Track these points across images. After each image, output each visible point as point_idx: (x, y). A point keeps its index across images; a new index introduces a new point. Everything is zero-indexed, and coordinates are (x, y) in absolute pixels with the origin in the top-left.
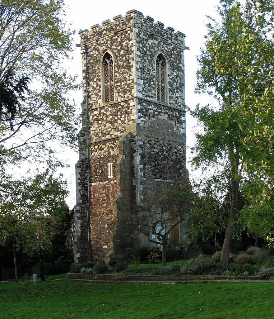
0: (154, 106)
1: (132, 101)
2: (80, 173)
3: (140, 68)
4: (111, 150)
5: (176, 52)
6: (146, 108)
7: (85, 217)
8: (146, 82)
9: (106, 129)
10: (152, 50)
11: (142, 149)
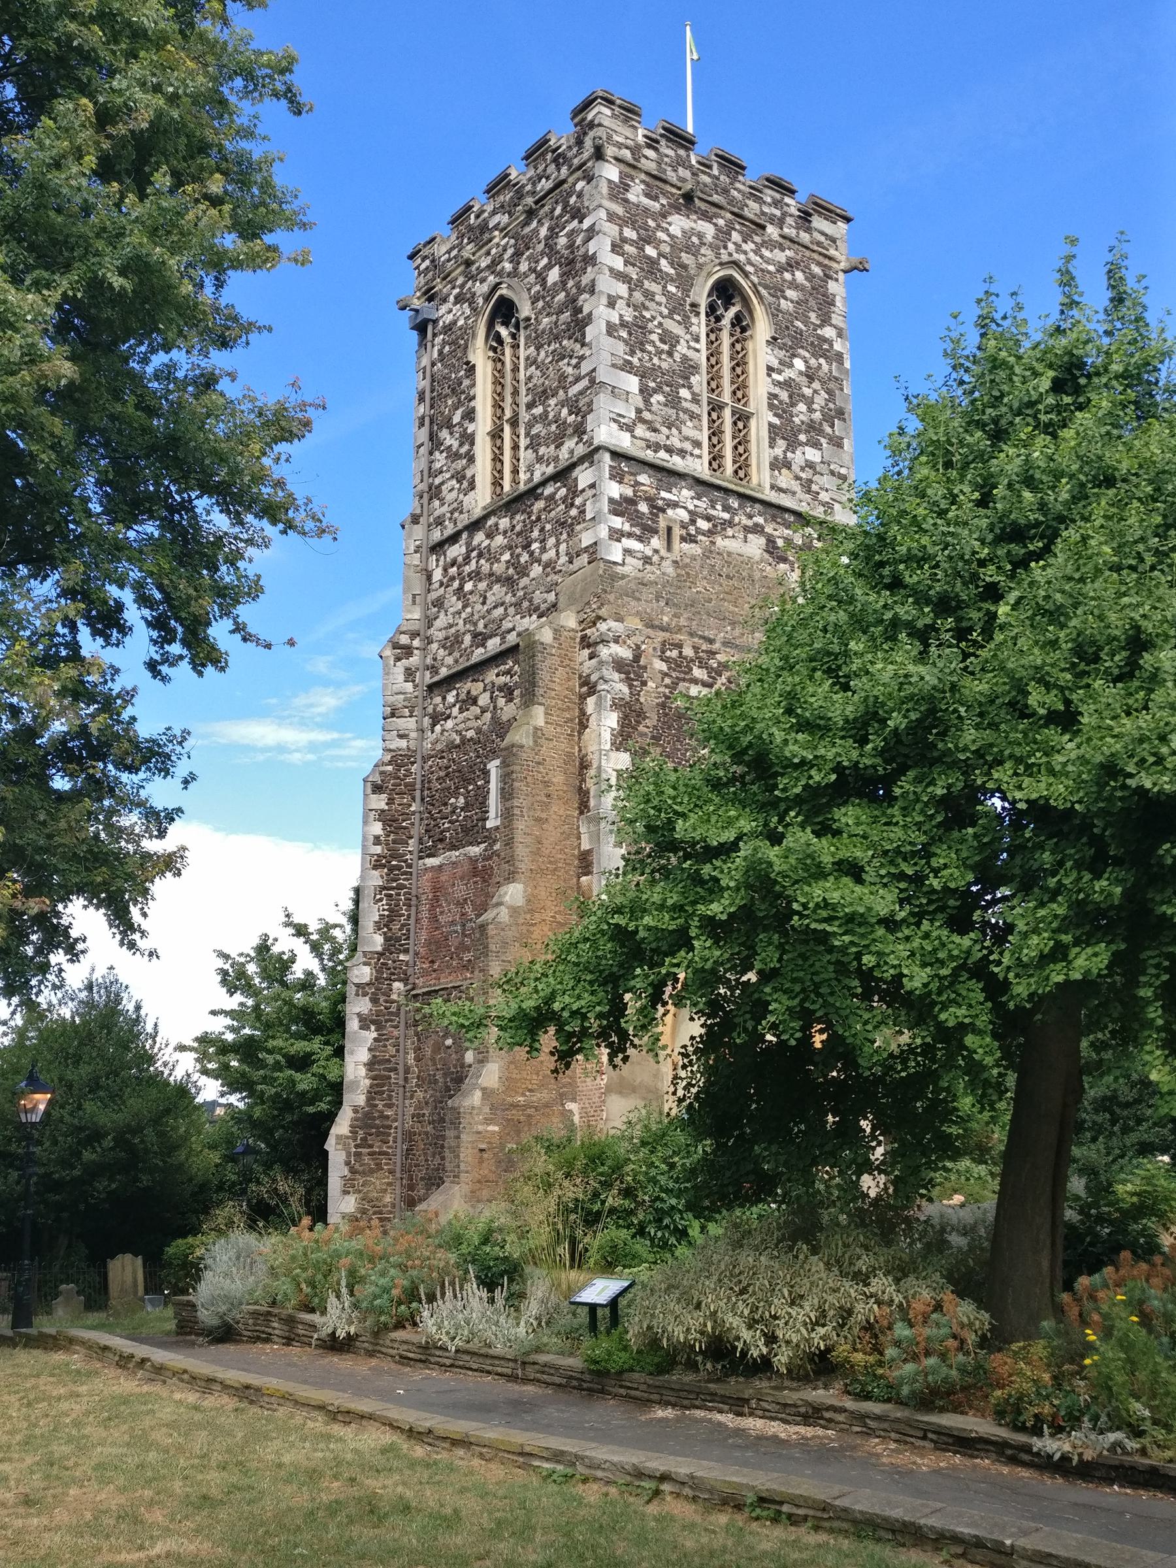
0: (692, 493)
1: (586, 464)
2: (382, 816)
3: (623, 324)
4: (501, 702)
5: (806, 279)
6: (650, 500)
7: (391, 1014)
8: (652, 385)
9: (488, 611)
10: (686, 258)
11: (628, 681)
